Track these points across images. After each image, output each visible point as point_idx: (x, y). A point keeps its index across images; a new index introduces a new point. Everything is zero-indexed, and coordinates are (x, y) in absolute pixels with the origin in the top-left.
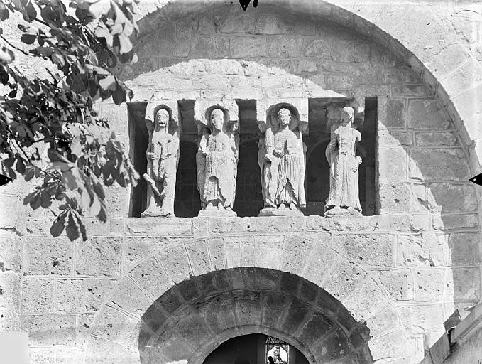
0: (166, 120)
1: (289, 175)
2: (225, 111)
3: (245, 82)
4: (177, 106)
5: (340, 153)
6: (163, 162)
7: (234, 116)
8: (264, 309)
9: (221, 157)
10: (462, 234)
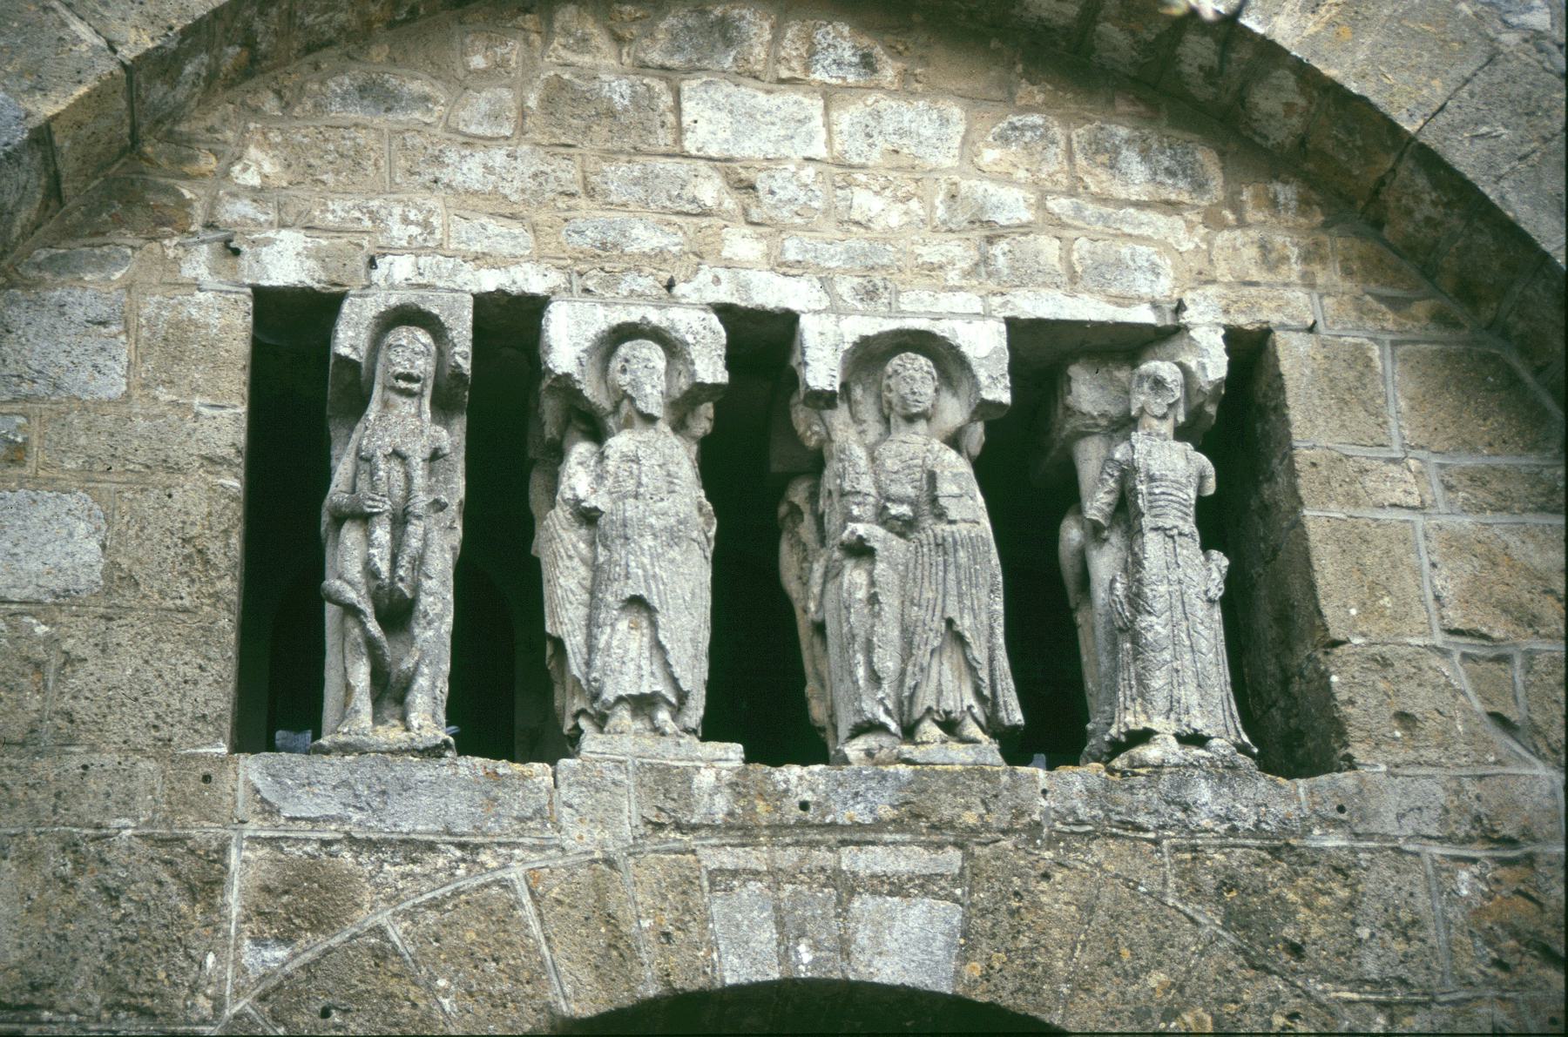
1: (952, 602)
3: (742, 244)
4: (468, 315)
5: (1146, 530)
6: (415, 528)
7: (711, 369)
9: (635, 544)
10: (668, 857)
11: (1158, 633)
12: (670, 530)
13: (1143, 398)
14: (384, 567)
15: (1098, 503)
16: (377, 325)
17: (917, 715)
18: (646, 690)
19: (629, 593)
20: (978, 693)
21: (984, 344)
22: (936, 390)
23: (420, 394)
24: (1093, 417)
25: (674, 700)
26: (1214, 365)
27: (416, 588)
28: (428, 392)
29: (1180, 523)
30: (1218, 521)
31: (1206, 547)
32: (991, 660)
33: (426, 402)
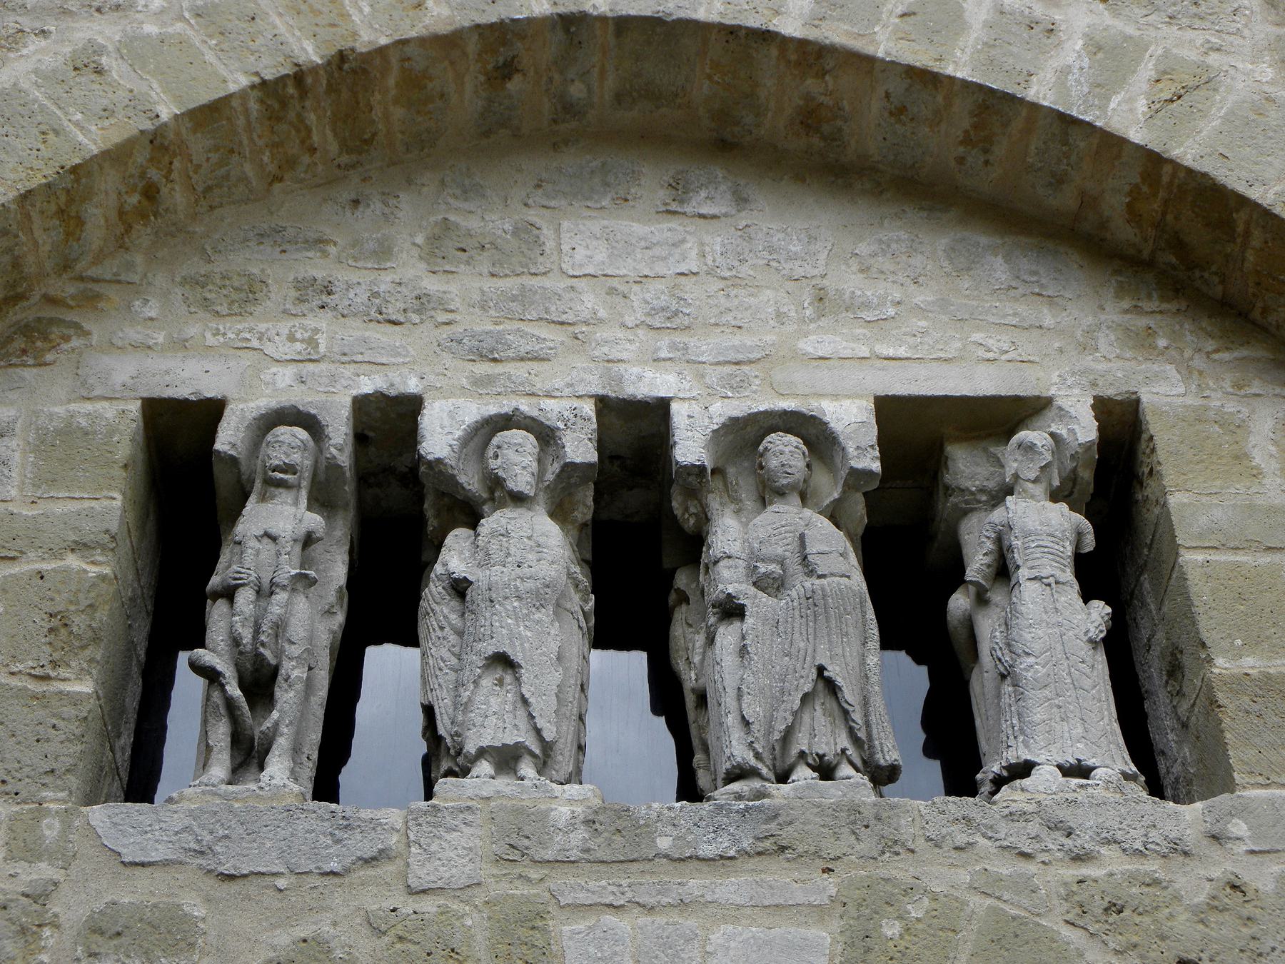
11: (1037, 672)
13: (1015, 465)
14: (246, 635)
15: (977, 563)
16: (259, 428)
19: (491, 650)
20: (852, 733)
21: (851, 419)
22: (808, 466)
23: (299, 487)
24: (972, 493)
25: (537, 752)
26: (1085, 430)
27: (279, 654)
28: (304, 483)
29: (1058, 573)
30: (1101, 572)
31: (1086, 597)
32: (865, 703)
33: (304, 494)
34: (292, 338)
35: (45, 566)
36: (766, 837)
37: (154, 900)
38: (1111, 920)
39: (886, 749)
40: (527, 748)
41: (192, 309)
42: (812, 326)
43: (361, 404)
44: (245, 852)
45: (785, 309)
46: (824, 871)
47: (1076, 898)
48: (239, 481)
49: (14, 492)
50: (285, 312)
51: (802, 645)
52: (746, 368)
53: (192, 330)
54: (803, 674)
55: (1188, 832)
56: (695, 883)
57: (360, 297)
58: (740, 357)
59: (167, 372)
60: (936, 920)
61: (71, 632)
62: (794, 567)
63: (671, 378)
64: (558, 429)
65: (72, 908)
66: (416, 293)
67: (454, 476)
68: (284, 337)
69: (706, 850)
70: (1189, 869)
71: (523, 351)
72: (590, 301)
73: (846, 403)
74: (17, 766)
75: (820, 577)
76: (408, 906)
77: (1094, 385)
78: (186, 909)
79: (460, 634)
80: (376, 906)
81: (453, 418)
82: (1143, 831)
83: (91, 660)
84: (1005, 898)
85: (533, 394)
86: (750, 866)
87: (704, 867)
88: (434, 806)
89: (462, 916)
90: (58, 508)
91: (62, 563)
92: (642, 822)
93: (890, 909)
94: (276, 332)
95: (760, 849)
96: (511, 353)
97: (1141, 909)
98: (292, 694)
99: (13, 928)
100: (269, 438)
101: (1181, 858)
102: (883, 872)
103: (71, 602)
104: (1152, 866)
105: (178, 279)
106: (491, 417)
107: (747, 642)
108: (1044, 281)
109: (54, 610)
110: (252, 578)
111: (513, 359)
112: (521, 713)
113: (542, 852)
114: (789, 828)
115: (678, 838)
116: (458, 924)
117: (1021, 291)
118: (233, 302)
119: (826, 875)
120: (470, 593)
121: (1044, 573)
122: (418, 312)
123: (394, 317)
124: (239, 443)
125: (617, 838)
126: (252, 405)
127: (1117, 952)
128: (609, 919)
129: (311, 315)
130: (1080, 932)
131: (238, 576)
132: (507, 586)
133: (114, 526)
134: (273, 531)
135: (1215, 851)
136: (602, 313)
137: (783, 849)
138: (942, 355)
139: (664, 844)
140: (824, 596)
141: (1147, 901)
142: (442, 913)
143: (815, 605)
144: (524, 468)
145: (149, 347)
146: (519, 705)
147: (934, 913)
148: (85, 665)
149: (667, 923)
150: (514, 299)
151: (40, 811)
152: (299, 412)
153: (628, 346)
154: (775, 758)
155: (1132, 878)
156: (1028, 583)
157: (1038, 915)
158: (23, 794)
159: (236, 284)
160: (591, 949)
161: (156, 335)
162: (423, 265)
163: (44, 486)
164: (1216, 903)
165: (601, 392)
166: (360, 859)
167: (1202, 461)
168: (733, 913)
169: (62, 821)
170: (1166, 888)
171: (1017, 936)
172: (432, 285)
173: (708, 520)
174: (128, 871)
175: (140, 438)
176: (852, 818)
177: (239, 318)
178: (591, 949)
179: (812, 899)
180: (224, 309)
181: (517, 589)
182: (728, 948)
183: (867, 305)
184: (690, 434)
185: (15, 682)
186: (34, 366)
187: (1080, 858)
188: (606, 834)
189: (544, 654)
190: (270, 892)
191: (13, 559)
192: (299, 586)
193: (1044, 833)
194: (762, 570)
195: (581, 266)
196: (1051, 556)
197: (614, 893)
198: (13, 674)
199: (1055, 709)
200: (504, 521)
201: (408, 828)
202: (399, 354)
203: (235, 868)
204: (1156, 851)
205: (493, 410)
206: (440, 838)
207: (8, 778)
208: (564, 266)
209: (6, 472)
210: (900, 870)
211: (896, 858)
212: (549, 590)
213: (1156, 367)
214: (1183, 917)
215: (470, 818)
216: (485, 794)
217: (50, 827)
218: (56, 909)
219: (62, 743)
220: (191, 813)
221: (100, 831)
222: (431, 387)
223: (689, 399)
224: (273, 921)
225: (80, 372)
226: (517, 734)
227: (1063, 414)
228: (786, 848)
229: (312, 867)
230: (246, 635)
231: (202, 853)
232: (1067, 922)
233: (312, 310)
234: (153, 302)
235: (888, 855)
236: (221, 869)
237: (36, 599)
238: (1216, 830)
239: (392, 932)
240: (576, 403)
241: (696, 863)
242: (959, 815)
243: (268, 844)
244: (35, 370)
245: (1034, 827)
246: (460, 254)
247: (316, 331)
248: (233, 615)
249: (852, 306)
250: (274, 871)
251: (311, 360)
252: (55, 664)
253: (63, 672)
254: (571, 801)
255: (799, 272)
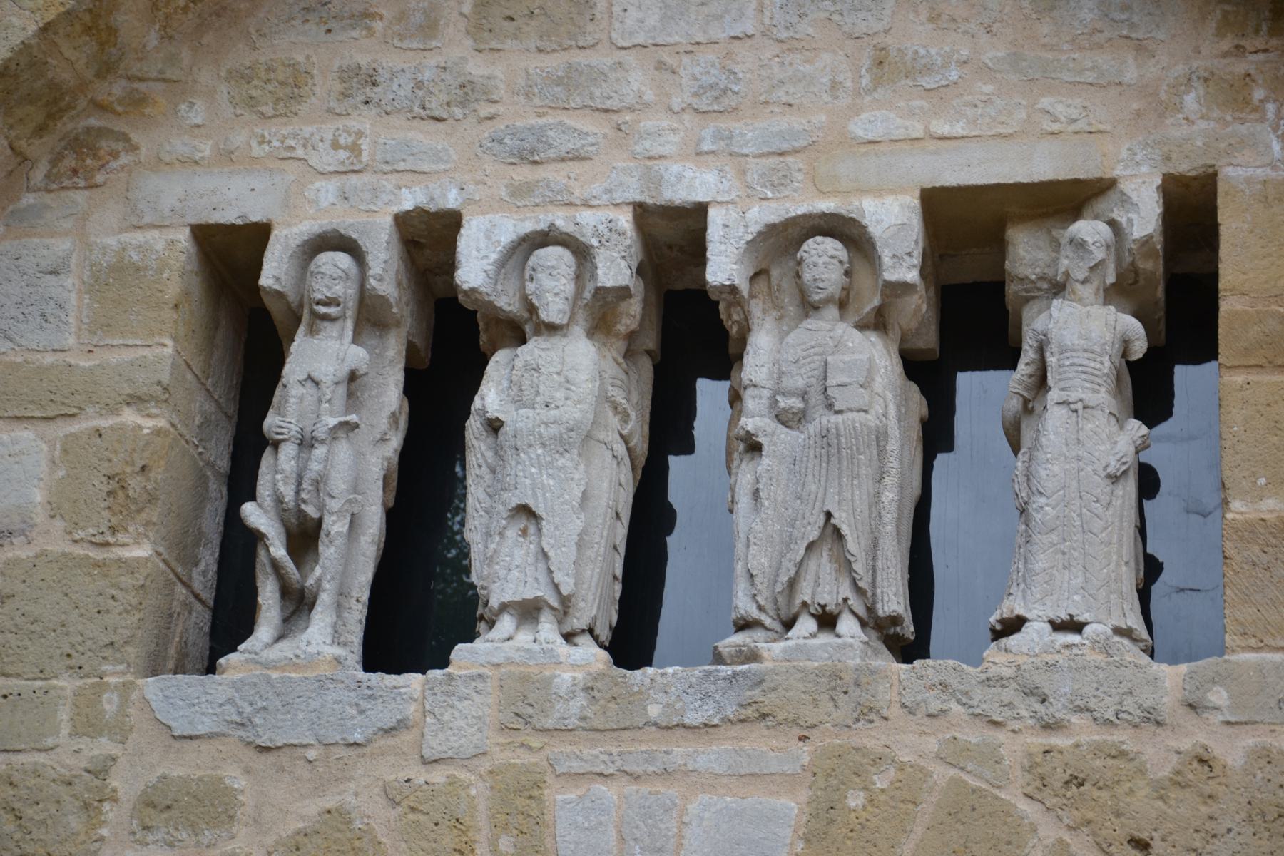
0: (345, 291)
2: (582, 253)
5: (1050, 404)
8: (205, 76)
11: (1046, 514)
12: (561, 440)
14: (288, 493)
16: (304, 253)
17: (794, 610)
18: (529, 595)
19: (514, 502)
21: (894, 221)
24: (1032, 282)
25: (555, 604)
26: (1144, 216)
27: (321, 507)
28: (349, 313)
34: (335, 145)
35: (103, 423)
36: (749, 704)
37: (199, 773)
38: (1069, 794)
39: (886, 599)
40: (545, 601)
41: (239, 112)
42: (868, 99)
43: (402, 221)
44: (281, 724)
45: (840, 78)
46: (800, 739)
47: (1039, 770)
48: (290, 308)
49: (72, 341)
50: (329, 110)
51: (813, 488)
52: (790, 159)
53: (239, 138)
54: (812, 520)
55: (1165, 700)
56: (680, 751)
57: (402, 88)
58: (785, 146)
59: (214, 192)
60: (898, 792)
61: (127, 496)
62: (816, 398)
63: (711, 177)
64: (592, 246)
65: (126, 784)
66: (461, 80)
67: (491, 303)
68: (328, 143)
69: (692, 718)
70: (1159, 739)
71: (564, 149)
72: (637, 81)
73: (889, 199)
74: (80, 639)
75: (837, 412)
76: (421, 775)
77: (1168, 158)
78: (227, 781)
79: (494, 471)
80: (393, 777)
81: (488, 238)
82: (1117, 699)
83: (147, 524)
84: (969, 768)
85: (571, 204)
86: (732, 733)
87: (689, 734)
88: (449, 675)
89: (468, 786)
90: (114, 358)
91: (117, 420)
92: (636, 689)
93: (857, 780)
94: (316, 133)
95: (742, 717)
96: (551, 153)
97: (1101, 784)
98: (332, 550)
99: (77, 803)
100: (312, 267)
101: (1153, 728)
102: (856, 741)
103: (127, 463)
104: (1122, 737)
105: (223, 74)
106: (527, 235)
107: (761, 486)
108: (1135, 19)
109: (111, 472)
110: (293, 433)
111: (554, 160)
112: (542, 565)
113: (543, 720)
114: (773, 695)
115: (668, 705)
116: (463, 794)
117: (1107, 34)
118: (278, 100)
119: (801, 744)
120: (502, 431)
121: (1073, 396)
122: (462, 104)
123: (436, 114)
124: (283, 277)
125: (612, 705)
126: (295, 230)
127: (1070, 828)
128: (600, 788)
129: (355, 114)
130: (1037, 806)
131: (279, 430)
132: (531, 433)
133: (165, 378)
134: (315, 375)
135: (1189, 719)
136: (649, 96)
137: (764, 716)
138: (1002, 130)
139: (654, 711)
140: (838, 435)
141: (1109, 774)
142: (450, 784)
143: (829, 445)
144: (556, 294)
145: (196, 162)
146: (540, 557)
147: (899, 784)
148: (141, 530)
149: (650, 793)
150: (559, 82)
151: (100, 688)
152: (341, 236)
153: (672, 138)
154: (778, 609)
155: (1097, 750)
156: (1056, 408)
157: (999, 787)
158: (86, 668)
159: (281, 78)
160: (580, 819)
161: (202, 147)
162: (469, 42)
163: (99, 332)
164: (1179, 778)
165: (639, 198)
166: (381, 729)
167: (1270, 255)
168: (710, 782)
169: (120, 696)
170: (1132, 760)
171: (974, 809)
172: (477, 68)
173: (749, 330)
174: (177, 744)
175: (194, 266)
176: (833, 683)
177: (285, 119)
178: (580, 819)
179: (785, 768)
180: (267, 109)
181: (541, 435)
182: (702, 819)
183: (928, 69)
184: (723, 247)
185: (78, 550)
186: (86, 188)
187: (1049, 726)
188: (602, 702)
189: (565, 503)
190: (301, 763)
191: (73, 415)
192: (341, 434)
193: (1018, 700)
194: (782, 405)
195: (631, 33)
196: (1084, 376)
197: (605, 762)
198: (75, 541)
199: (1060, 556)
200: (537, 352)
201: (424, 698)
202: (440, 160)
203: (271, 741)
204: (1127, 721)
205: (528, 227)
206: (452, 707)
207: (73, 652)
208: (614, 35)
209: (63, 317)
210: (871, 738)
211: (870, 726)
212: (573, 434)
213: (1243, 129)
214: (1143, 793)
215: (480, 686)
216: (496, 660)
217: (110, 701)
218: (115, 784)
219: (120, 614)
220: (234, 685)
221: (153, 705)
222: (469, 201)
223: (727, 202)
224: (303, 791)
225: (129, 195)
226: (540, 590)
227: (1125, 200)
228: (768, 715)
229: (338, 738)
230: (288, 493)
231: (243, 725)
232: (1026, 795)
233: (356, 108)
234: (200, 105)
235: (862, 722)
236: (259, 742)
237: (95, 460)
238: (1193, 698)
239: (405, 803)
240: (611, 213)
241: (682, 730)
242: (936, 681)
243: (301, 716)
244: (87, 193)
245: (1009, 694)
246: (507, 24)
247: (360, 134)
248: (277, 472)
249: (914, 69)
250: (305, 742)
251: (354, 171)
252: (114, 530)
253: (122, 537)
254: (575, 667)
255: (862, 27)
